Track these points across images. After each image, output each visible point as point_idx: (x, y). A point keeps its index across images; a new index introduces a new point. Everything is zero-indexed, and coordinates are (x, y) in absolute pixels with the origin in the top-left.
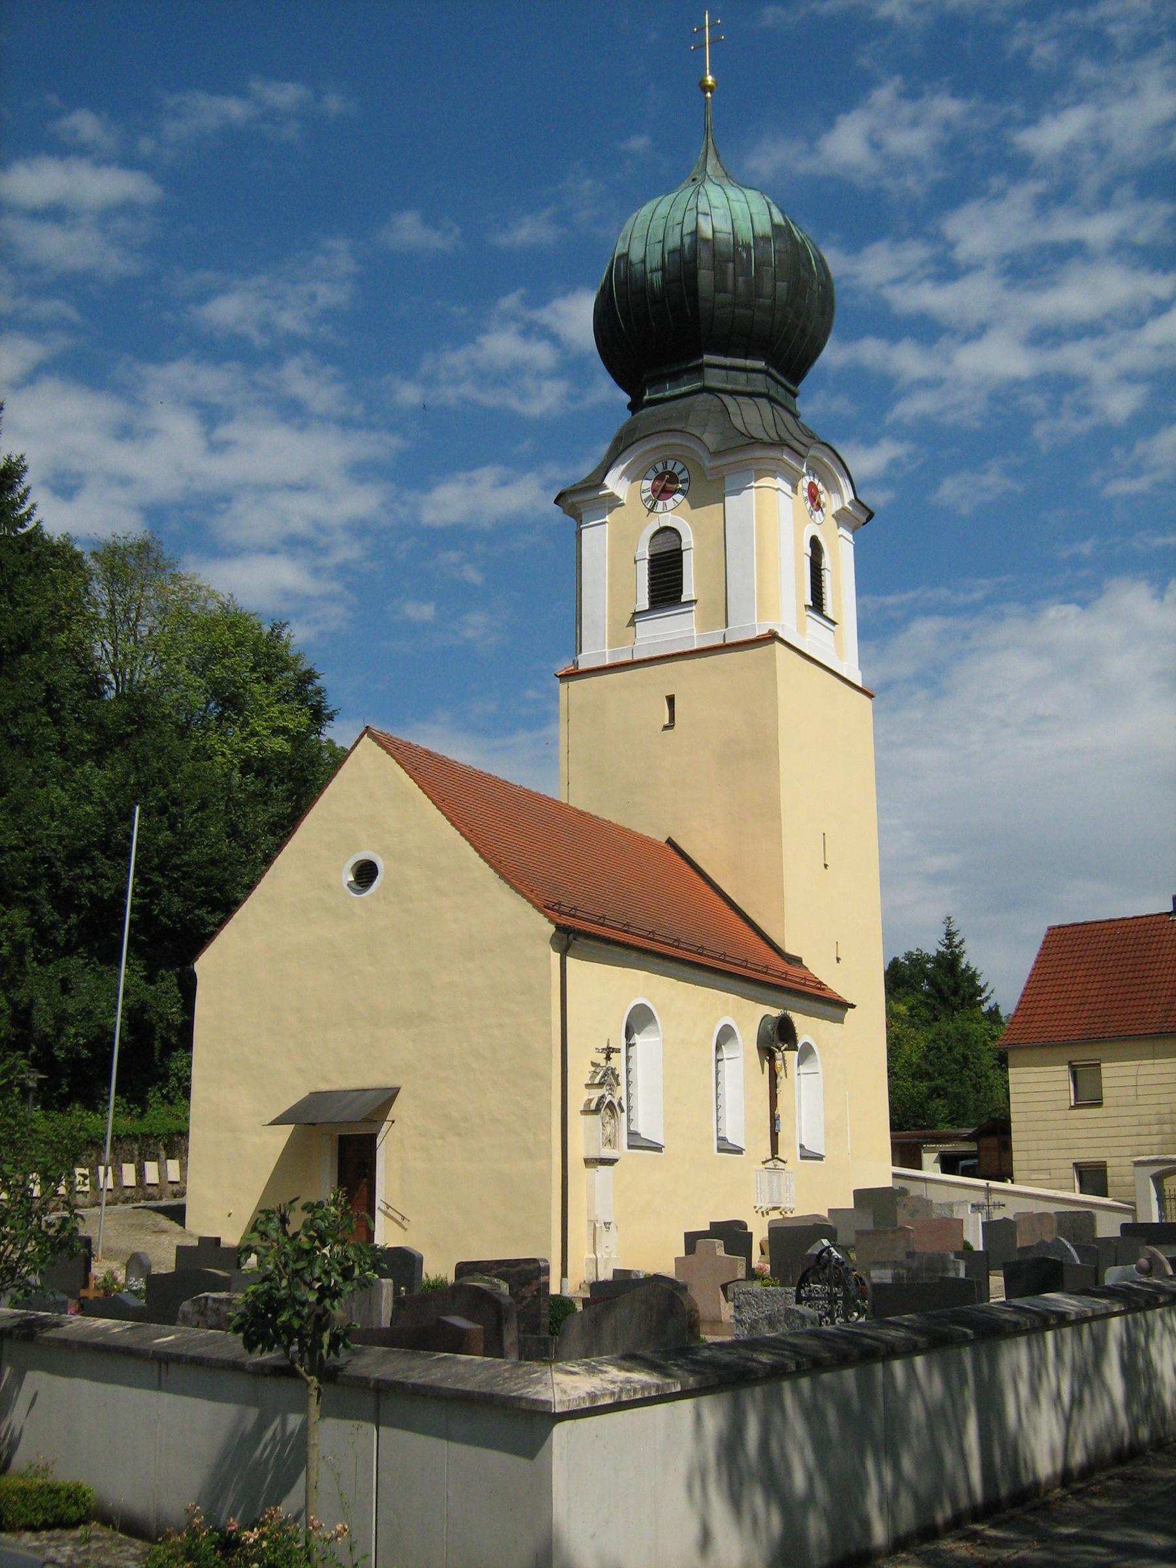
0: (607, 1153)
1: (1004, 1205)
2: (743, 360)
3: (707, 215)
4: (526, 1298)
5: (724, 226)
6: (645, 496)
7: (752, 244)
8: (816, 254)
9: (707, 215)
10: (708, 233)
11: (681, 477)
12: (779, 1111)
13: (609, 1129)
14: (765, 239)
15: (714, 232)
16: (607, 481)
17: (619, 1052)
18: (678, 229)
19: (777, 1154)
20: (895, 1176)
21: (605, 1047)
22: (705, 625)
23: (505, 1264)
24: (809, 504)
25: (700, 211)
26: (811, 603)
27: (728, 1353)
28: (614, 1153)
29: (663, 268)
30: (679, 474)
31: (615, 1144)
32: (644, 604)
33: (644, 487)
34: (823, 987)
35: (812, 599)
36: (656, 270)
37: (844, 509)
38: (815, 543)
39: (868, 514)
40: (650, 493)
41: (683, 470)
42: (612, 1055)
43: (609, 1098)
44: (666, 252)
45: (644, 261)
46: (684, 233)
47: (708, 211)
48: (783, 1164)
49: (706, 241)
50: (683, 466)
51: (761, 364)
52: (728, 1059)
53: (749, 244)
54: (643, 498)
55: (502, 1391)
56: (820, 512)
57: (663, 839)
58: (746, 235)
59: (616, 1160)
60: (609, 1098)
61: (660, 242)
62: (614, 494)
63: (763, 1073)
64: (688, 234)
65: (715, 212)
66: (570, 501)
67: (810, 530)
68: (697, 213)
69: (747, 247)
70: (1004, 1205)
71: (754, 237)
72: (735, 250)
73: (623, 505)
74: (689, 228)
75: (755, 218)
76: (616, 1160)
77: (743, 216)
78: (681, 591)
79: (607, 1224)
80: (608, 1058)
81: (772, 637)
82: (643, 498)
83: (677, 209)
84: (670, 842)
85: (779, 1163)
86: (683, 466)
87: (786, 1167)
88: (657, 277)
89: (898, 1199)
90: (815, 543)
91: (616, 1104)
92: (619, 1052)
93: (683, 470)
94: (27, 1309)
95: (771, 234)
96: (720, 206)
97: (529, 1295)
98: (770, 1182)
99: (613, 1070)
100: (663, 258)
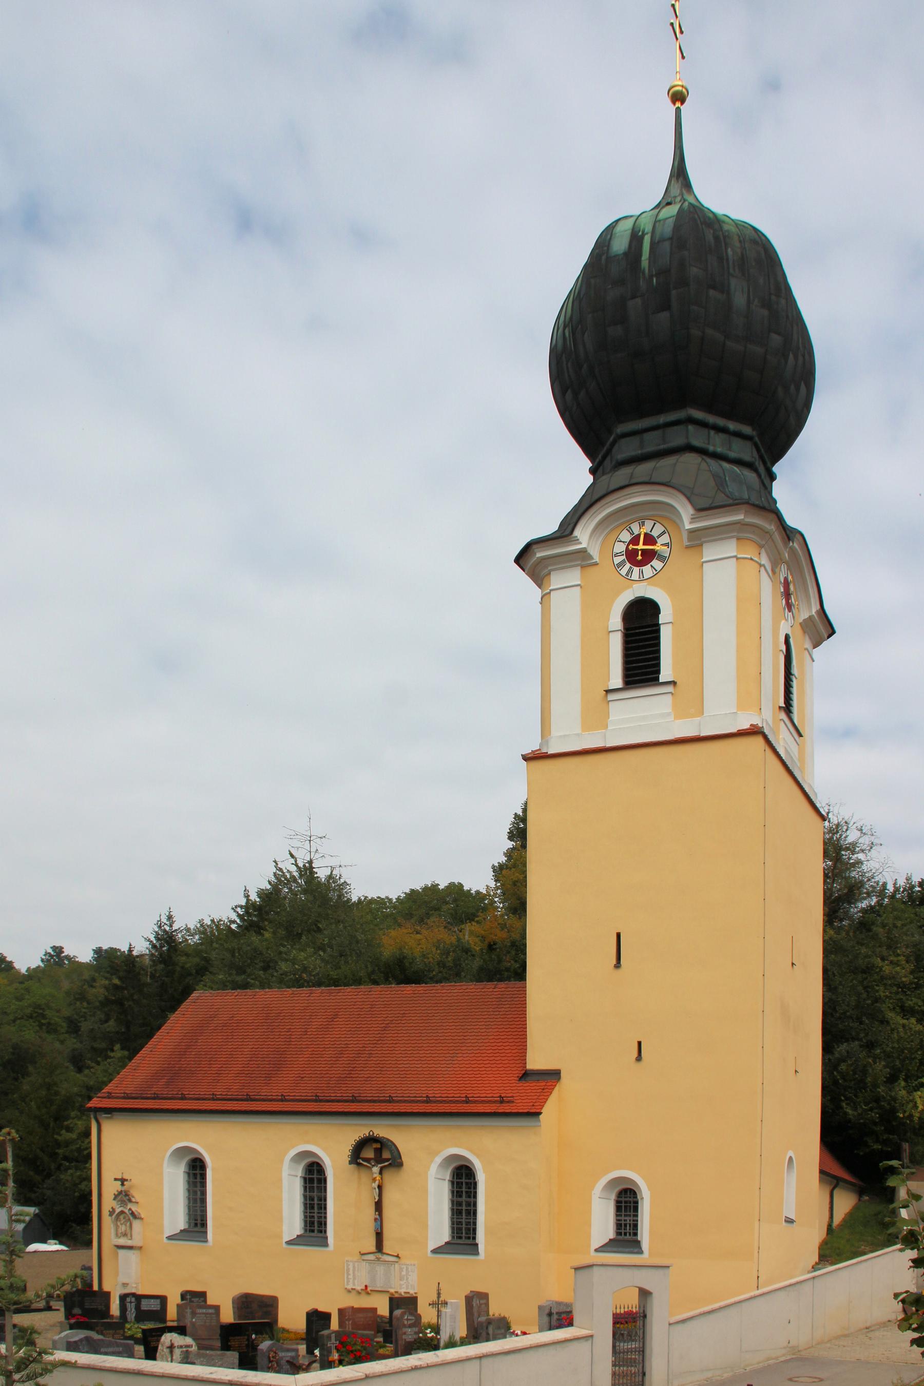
2: (284, 1202)
6: (617, 560)
16: (577, 533)
27: (409, 1293)
31: (131, 1236)
32: (617, 681)
33: (616, 550)
37: (811, 618)
40: (624, 557)
50: (663, 529)
51: (747, 430)
54: (616, 563)
55: (64, 1022)
62: (587, 551)
67: (785, 628)
73: (596, 564)
78: (658, 672)
82: (616, 563)
86: (663, 529)
94: (61, 1337)
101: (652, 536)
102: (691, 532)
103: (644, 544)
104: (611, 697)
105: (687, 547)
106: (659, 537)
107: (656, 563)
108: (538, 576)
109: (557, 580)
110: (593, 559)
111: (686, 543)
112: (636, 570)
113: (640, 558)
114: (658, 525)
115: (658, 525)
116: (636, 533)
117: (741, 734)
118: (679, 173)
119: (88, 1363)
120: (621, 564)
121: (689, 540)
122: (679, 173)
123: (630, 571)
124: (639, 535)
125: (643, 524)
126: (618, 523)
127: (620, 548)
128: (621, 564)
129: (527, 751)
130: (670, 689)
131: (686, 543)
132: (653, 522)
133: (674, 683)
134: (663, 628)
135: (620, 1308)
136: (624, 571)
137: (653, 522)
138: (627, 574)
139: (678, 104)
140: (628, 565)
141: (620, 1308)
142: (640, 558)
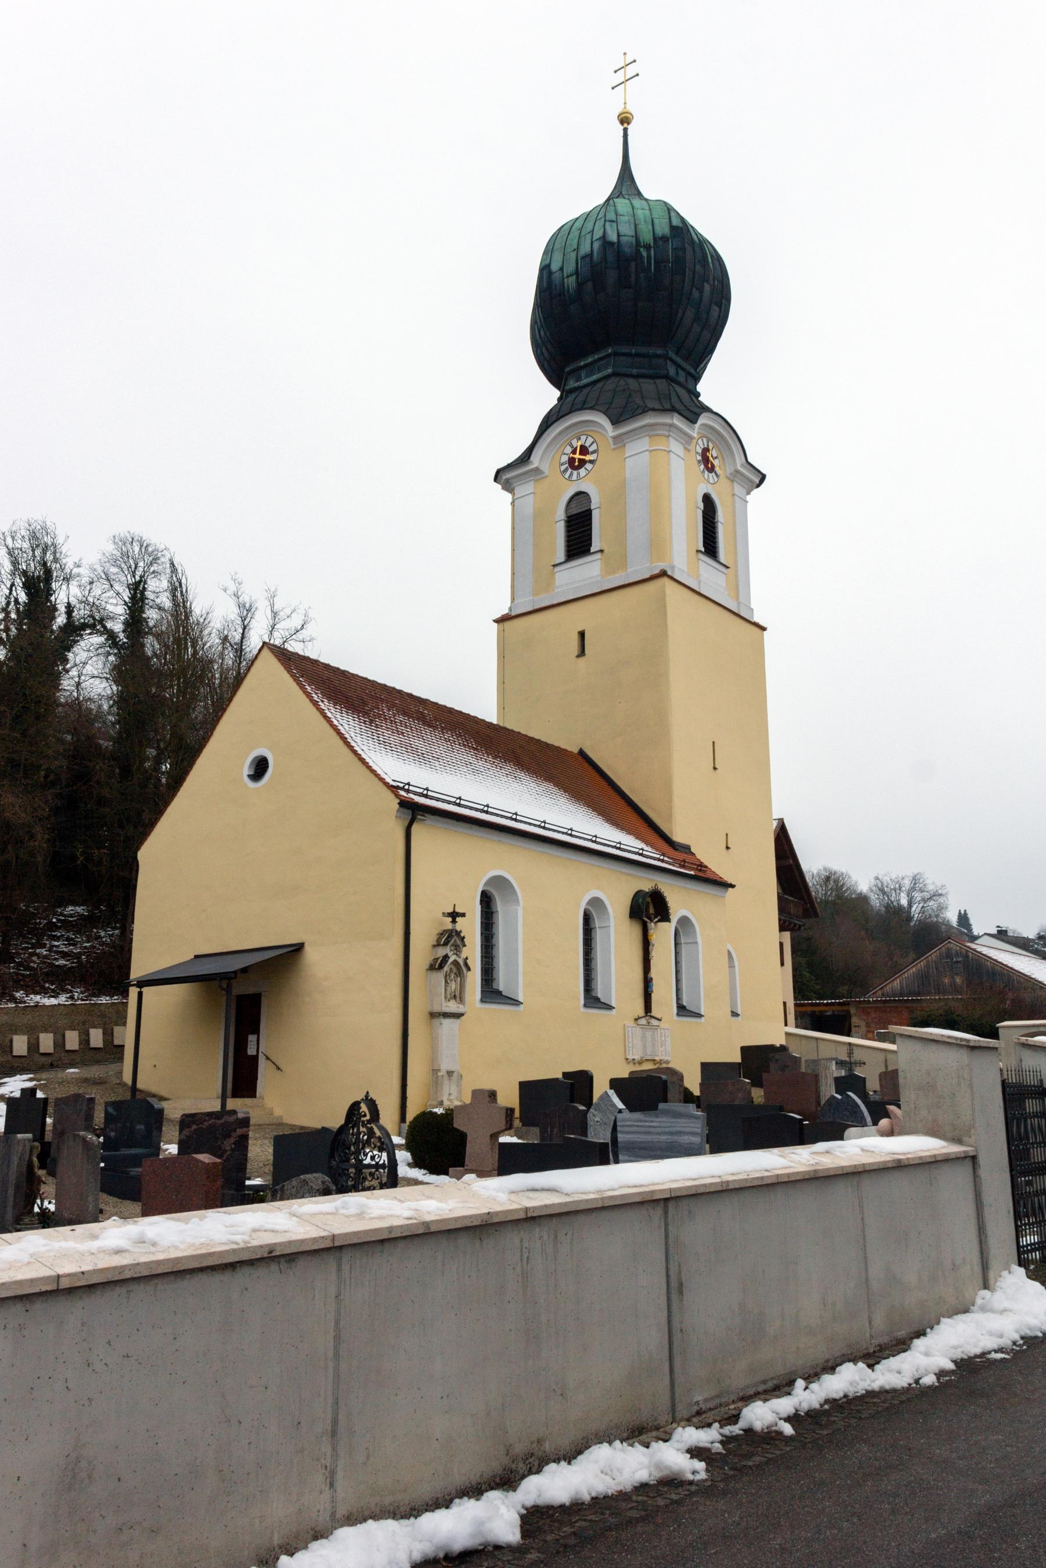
0: (452, 1007)
1: (864, 1063)
3: (614, 222)
4: (227, 1151)
5: (627, 230)
6: (563, 468)
7: (652, 244)
8: (714, 254)
9: (614, 222)
10: (613, 237)
11: (591, 449)
12: (653, 974)
13: (453, 986)
14: (664, 239)
15: (619, 236)
17: (465, 916)
18: (589, 237)
19: (651, 1012)
20: (787, 1034)
21: (451, 910)
22: (609, 569)
23: (214, 1116)
24: (702, 467)
25: (607, 219)
26: (703, 550)
28: (458, 1007)
29: (577, 273)
30: (590, 446)
32: (561, 554)
34: (705, 869)
35: (704, 546)
36: (571, 275)
38: (707, 500)
39: (761, 476)
40: (567, 465)
41: (593, 443)
42: (458, 919)
43: (452, 958)
44: (579, 258)
45: (561, 269)
46: (594, 239)
47: (614, 218)
48: (658, 1021)
49: (611, 244)
50: (593, 440)
52: (685, 943)
53: (650, 245)
56: (713, 474)
57: (576, 751)
58: (647, 237)
59: (462, 1015)
60: (452, 958)
61: (574, 250)
63: (782, 964)
64: (597, 240)
65: (621, 219)
66: (504, 478)
67: (702, 489)
68: (605, 221)
69: (648, 247)
70: (864, 1063)
71: (655, 238)
72: (638, 252)
74: (598, 234)
75: (656, 222)
76: (462, 1015)
77: (645, 221)
79: (450, 1073)
80: (454, 921)
81: (663, 574)
83: (590, 221)
84: (582, 753)
85: (654, 1022)
86: (593, 440)
87: (662, 1024)
88: (571, 282)
89: (771, 1055)
90: (707, 500)
91: (462, 964)
92: (465, 916)
93: (593, 443)
95: (669, 235)
96: (625, 214)
97: (229, 1148)
98: (644, 1037)
99: (458, 933)
100: (577, 264)
101: (585, 447)
102: (614, 438)
103: (580, 454)
104: (557, 569)
105: (614, 449)
106: (590, 446)
107: (588, 466)
108: (508, 487)
109: (520, 491)
110: (544, 473)
111: (613, 447)
112: (575, 473)
113: (577, 464)
114: (589, 437)
115: (589, 437)
116: (575, 446)
117: (653, 578)
118: (626, 175)
119: (675, 1372)
120: (566, 470)
121: (614, 444)
122: (626, 175)
123: (571, 474)
124: (577, 447)
125: (580, 439)
126: (558, 446)
127: (565, 458)
128: (566, 470)
129: (498, 615)
130: (598, 556)
131: (613, 447)
132: (585, 437)
133: (601, 551)
134: (594, 513)
135: (1011, 1071)
136: (567, 476)
137: (585, 437)
138: (569, 477)
139: (625, 125)
140: (570, 470)
141: (1011, 1071)
142: (577, 464)
